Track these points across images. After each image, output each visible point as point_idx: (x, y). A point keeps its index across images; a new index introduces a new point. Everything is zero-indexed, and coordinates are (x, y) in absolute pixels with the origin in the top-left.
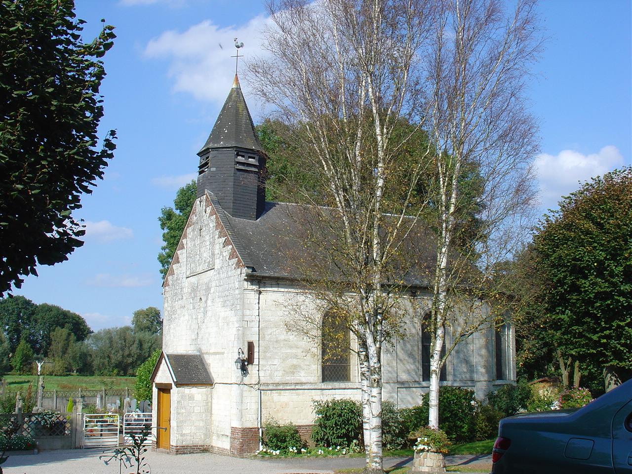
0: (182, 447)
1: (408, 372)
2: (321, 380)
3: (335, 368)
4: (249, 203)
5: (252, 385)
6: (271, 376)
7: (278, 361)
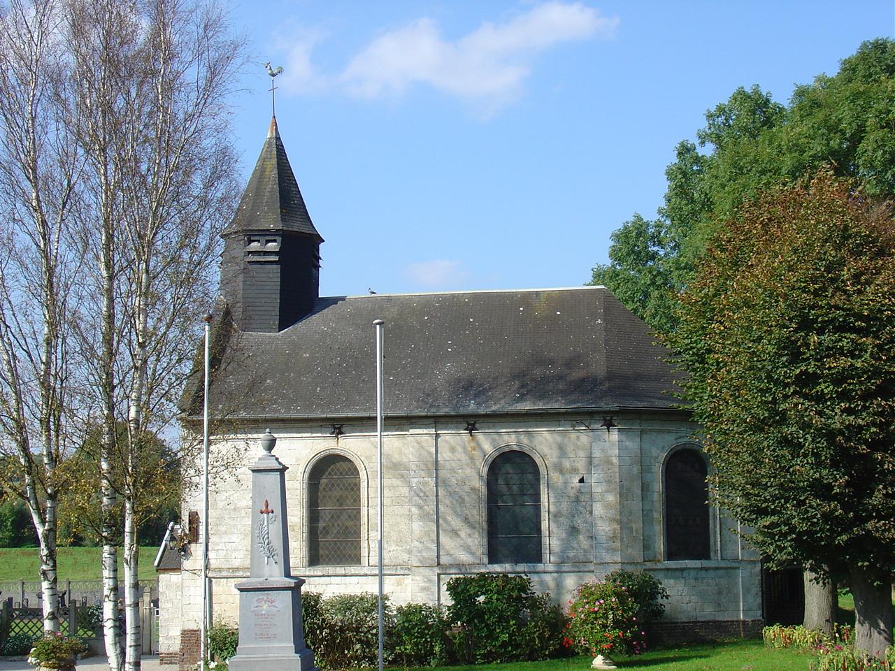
0: (168, 654)
1: (467, 549)
2: (306, 560)
3: (336, 544)
4: (268, 309)
5: (196, 571)
6: (226, 558)
7: (238, 537)
